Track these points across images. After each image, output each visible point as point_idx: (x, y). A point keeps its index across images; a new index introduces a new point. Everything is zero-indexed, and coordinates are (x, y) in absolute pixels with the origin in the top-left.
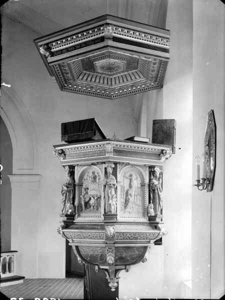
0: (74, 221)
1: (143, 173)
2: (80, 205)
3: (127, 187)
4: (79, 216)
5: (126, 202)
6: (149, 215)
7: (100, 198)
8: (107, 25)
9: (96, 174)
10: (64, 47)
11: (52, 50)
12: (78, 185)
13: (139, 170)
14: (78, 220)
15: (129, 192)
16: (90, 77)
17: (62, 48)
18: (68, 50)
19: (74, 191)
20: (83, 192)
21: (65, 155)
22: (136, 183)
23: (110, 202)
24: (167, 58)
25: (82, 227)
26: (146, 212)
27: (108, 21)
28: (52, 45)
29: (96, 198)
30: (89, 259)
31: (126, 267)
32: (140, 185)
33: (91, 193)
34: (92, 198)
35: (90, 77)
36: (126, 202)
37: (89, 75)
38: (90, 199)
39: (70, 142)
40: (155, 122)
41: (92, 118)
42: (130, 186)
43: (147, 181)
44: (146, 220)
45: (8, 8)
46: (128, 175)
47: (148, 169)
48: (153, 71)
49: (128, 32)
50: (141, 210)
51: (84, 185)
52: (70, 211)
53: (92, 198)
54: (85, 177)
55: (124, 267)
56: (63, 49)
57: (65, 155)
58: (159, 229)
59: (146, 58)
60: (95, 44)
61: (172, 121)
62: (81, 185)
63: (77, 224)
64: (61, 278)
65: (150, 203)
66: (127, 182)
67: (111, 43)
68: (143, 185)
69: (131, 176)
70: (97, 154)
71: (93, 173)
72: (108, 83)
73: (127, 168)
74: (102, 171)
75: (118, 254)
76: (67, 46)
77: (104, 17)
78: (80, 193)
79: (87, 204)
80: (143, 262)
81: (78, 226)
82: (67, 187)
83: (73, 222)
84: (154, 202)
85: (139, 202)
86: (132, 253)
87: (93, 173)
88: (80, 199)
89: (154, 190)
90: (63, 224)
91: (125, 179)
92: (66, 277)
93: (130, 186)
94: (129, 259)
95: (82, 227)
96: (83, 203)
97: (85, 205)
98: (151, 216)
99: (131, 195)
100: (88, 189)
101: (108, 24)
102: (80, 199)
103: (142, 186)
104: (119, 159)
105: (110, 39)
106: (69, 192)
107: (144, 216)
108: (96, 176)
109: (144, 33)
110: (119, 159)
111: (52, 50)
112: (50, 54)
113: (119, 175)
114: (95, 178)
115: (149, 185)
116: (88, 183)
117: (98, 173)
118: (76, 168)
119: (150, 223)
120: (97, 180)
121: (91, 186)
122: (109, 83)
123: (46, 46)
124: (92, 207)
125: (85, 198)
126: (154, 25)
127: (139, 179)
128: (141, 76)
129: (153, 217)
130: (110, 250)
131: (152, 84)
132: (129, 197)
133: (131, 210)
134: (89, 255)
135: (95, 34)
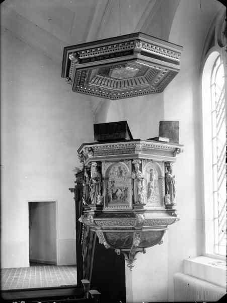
0: (103, 211)
1: (161, 168)
2: (107, 197)
3: (148, 181)
4: (107, 206)
5: (149, 193)
6: (166, 204)
7: (126, 190)
8: (138, 41)
9: (122, 169)
10: (93, 56)
11: (80, 58)
12: (106, 179)
13: (158, 166)
14: (106, 209)
15: (151, 184)
16: (104, 80)
17: (91, 56)
18: (96, 59)
19: (102, 184)
20: (110, 185)
21: (93, 152)
22: (155, 177)
23: (139, 193)
24: (179, 70)
25: (112, 215)
26: (163, 201)
27: (140, 38)
28: (81, 53)
29: (123, 190)
30: (115, 243)
31: (143, 249)
32: (157, 179)
33: (117, 185)
34: (119, 190)
35: (104, 80)
36: (149, 193)
37: (106, 80)
38: (117, 190)
39: (100, 142)
40: (161, 123)
41: (122, 120)
42: (151, 179)
43: (163, 175)
44: (163, 208)
45: (8, 7)
46: (149, 170)
47: (164, 164)
48: (159, 78)
49: (147, 45)
50: (159, 200)
51: (110, 179)
52: (100, 202)
53: (119, 190)
54: (111, 171)
55: (141, 249)
56: (92, 58)
57: (93, 152)
58: (175, 215)
59: (160, 68)
60: (124, 55)
61: (178, 122)
62: (107, 179)
63: (105, 214)
64: (23, 266)
65: (166, 193)
66: (148, 176)
67: (139, 56)
68: (160, 178)
69: (151, 170)
70: (126, 151)
71: (119, 168)
72: (114, 87)
73: (148, 164)
74: (129, 167)
75: (143, 238)
76: (95, 55)
77: (136, 34)
78: (107, 186)
79: (114, 195)
80: (160, 244)
81: (108, 215)
82: (97, 181)
83: (102, 212)
84: (170, 192)
85: (158, 193)
86: (153, 237)
87: (119, 168)
88: (107, 190)
89: (170, 183)
90: (174, 208)
91: (147, 174)
92: (30, 266)
93: (151, 179)
94: (149, 242)
95: (112, 215)
96: (111, 195)
97: (112, 197)
98: (168, 205)
99: (152, 187)
100: (114, 182)
101: (139, 40)
102: (107, 190)
103: (159, 179)
104: (145, 156)
105: (139, 52)
106: (98, 184)
107: (162, 205)
108: (122, 171)
109: (155, 45)
110: (145, 156)
111: (80, 58)
112: (79, 61)
113: (144, 170)
114: (121, 172)
115: (165, 178)
116: (114, 175)
117: (124, 168)
118: (103, 163)
119: (167, 211)
120: (123, 175)
121: (117, 180)
122: (115, 86)
123: (76, 54)
124: (119, 198)
125: (112, 190)
126: (159, 38)
127: (157, 173)
128: (146, 82)
129: (170, 205)
130: (137, 235)
131: (153, 88)
132: (151, 188)
133: (152, 200)
134: (116, 239)
135: (125, 47)
